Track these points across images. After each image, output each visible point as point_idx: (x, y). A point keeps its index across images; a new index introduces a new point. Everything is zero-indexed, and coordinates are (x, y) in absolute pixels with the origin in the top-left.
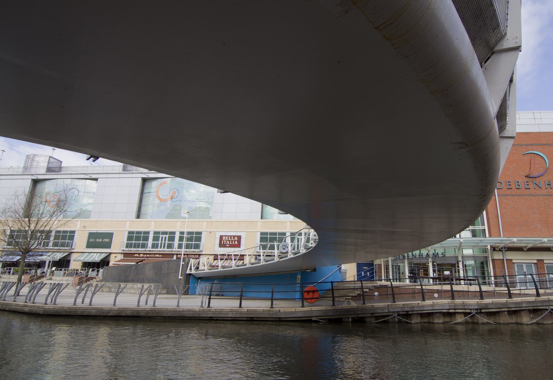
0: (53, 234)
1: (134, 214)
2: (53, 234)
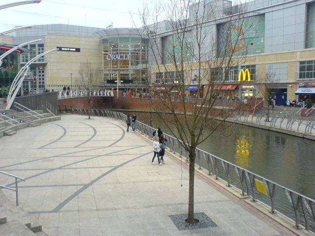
0: (164, 75)
1: (302, 44)
2: (164, 75)
